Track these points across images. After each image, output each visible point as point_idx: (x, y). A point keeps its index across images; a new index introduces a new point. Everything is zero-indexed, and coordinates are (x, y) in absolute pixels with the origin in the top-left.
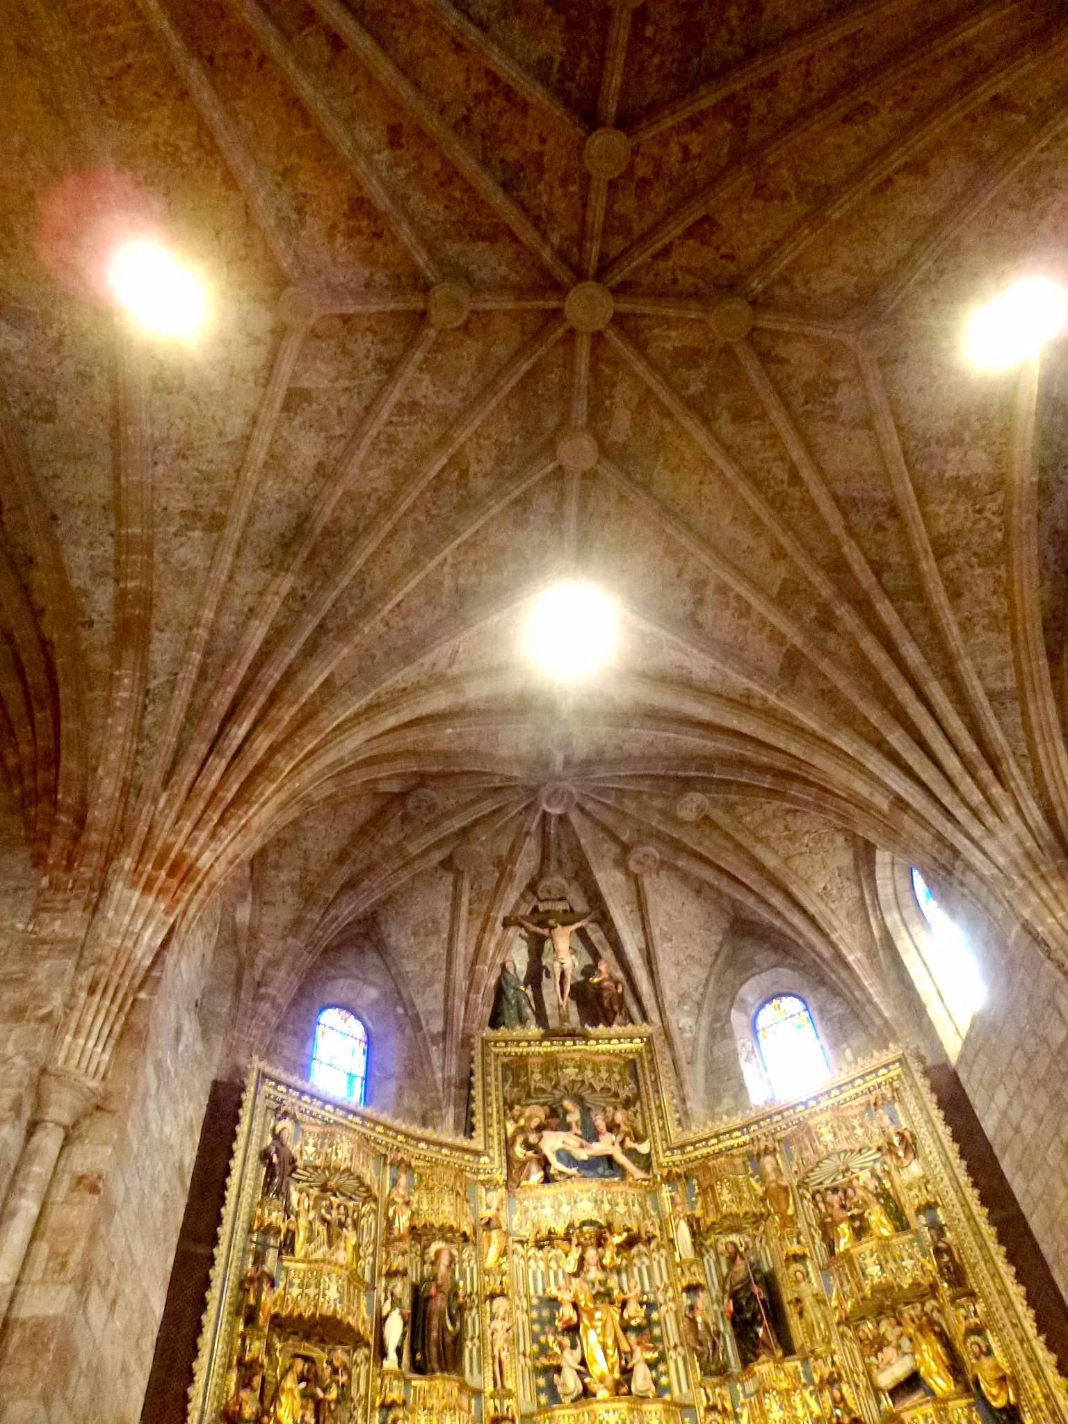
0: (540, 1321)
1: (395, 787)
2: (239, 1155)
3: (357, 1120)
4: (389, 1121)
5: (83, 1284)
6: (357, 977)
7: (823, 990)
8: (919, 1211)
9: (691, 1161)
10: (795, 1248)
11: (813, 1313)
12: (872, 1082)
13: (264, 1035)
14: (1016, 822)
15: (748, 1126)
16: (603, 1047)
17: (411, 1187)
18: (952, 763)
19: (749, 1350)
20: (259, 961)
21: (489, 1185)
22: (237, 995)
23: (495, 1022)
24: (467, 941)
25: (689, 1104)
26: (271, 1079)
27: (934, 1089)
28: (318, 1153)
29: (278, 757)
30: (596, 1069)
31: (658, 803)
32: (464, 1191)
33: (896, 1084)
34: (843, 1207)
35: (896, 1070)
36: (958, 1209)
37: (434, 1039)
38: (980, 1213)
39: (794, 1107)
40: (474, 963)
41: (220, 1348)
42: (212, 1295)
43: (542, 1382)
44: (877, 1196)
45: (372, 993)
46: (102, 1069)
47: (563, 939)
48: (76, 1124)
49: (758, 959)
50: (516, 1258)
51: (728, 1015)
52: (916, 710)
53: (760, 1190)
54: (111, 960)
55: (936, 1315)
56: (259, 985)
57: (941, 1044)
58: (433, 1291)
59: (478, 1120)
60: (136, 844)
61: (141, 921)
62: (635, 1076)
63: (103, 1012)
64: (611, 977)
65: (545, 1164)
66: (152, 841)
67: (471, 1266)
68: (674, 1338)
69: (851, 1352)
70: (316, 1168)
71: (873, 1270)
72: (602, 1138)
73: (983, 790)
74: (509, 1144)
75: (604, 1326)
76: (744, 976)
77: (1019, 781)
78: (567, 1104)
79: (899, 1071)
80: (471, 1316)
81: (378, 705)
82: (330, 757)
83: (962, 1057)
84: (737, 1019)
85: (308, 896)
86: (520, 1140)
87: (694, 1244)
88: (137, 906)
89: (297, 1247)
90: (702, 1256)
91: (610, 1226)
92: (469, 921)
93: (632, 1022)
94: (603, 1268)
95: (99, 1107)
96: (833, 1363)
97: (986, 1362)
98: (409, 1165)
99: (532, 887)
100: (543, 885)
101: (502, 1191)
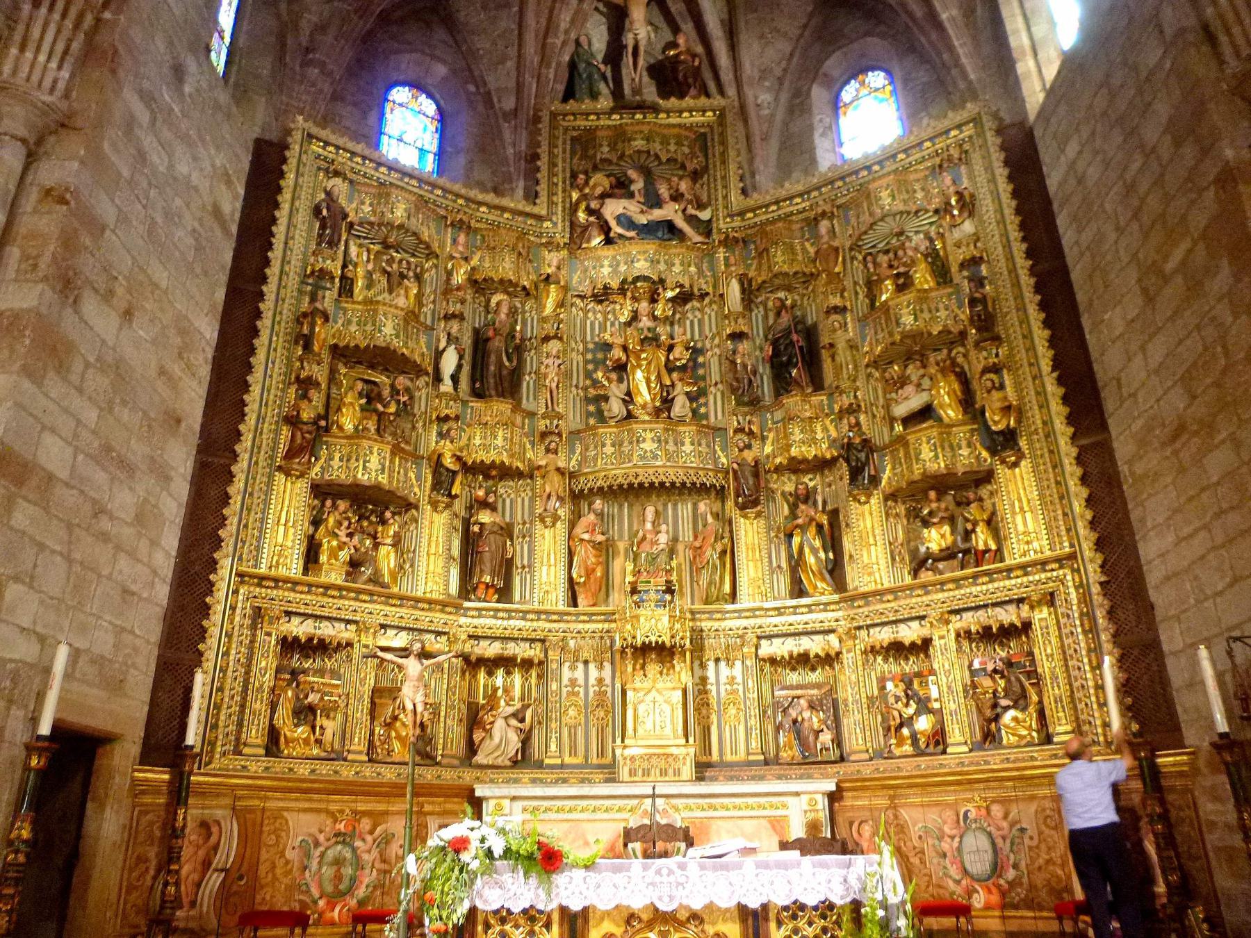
0: (595, 362)
3: (414, 182)
4: (448, 185)
6: (423, 52)
7: (911, 57)
8: (962, 266)
10: (836, 301)
11: (843, 354)
12: (940, 144)
15: (808, 193)
16: (674, 120)
17: (471, 248)
19: (782, 384)
21: (551, 245)
22: (281, 59)
23: (569, 95)
24: (537, 15)
25: (757, 177)
26: (319, 140)
27: (1003, 148)
28: (374, 212)
30: (665, 141)
32: (526, 253)
33: (966, 147)
34: (891, 267)
37: (507, 116)
38: (1023, 264)
39: (856, 172)
41: (277, 370)
42: (264, 324)
43: (592, 408)
44: (926, 256)
45: (441, 70)
46: (61, 85)
51: (810, 89)
53: (812, 250)
55: (960, 360)
56: (308, 50)
57: (1023, 101)
58: (491, 333)
59: (543, 188)
64: (688, 51)
65: (605, 229)
67: (532, 316)
68: (715, 376)
69: (875, 390)
70: (371, 224)
74: (574, 209)
75: (649, 364)
76: (831, 49)
78: (632, 174)
79: (972, 132)
80: (530, 357)
83: (1043, 112)
84: (818, 94)
86: (583, 206)
87: (743, 299)
89: (356, 291)
90: (751, 310)
91: (662, 281)
93: (708, 96)
94: (655, 318)
96: (856, 397)
97: (996, 395)
98: (469, 227)
101: (564, 253)
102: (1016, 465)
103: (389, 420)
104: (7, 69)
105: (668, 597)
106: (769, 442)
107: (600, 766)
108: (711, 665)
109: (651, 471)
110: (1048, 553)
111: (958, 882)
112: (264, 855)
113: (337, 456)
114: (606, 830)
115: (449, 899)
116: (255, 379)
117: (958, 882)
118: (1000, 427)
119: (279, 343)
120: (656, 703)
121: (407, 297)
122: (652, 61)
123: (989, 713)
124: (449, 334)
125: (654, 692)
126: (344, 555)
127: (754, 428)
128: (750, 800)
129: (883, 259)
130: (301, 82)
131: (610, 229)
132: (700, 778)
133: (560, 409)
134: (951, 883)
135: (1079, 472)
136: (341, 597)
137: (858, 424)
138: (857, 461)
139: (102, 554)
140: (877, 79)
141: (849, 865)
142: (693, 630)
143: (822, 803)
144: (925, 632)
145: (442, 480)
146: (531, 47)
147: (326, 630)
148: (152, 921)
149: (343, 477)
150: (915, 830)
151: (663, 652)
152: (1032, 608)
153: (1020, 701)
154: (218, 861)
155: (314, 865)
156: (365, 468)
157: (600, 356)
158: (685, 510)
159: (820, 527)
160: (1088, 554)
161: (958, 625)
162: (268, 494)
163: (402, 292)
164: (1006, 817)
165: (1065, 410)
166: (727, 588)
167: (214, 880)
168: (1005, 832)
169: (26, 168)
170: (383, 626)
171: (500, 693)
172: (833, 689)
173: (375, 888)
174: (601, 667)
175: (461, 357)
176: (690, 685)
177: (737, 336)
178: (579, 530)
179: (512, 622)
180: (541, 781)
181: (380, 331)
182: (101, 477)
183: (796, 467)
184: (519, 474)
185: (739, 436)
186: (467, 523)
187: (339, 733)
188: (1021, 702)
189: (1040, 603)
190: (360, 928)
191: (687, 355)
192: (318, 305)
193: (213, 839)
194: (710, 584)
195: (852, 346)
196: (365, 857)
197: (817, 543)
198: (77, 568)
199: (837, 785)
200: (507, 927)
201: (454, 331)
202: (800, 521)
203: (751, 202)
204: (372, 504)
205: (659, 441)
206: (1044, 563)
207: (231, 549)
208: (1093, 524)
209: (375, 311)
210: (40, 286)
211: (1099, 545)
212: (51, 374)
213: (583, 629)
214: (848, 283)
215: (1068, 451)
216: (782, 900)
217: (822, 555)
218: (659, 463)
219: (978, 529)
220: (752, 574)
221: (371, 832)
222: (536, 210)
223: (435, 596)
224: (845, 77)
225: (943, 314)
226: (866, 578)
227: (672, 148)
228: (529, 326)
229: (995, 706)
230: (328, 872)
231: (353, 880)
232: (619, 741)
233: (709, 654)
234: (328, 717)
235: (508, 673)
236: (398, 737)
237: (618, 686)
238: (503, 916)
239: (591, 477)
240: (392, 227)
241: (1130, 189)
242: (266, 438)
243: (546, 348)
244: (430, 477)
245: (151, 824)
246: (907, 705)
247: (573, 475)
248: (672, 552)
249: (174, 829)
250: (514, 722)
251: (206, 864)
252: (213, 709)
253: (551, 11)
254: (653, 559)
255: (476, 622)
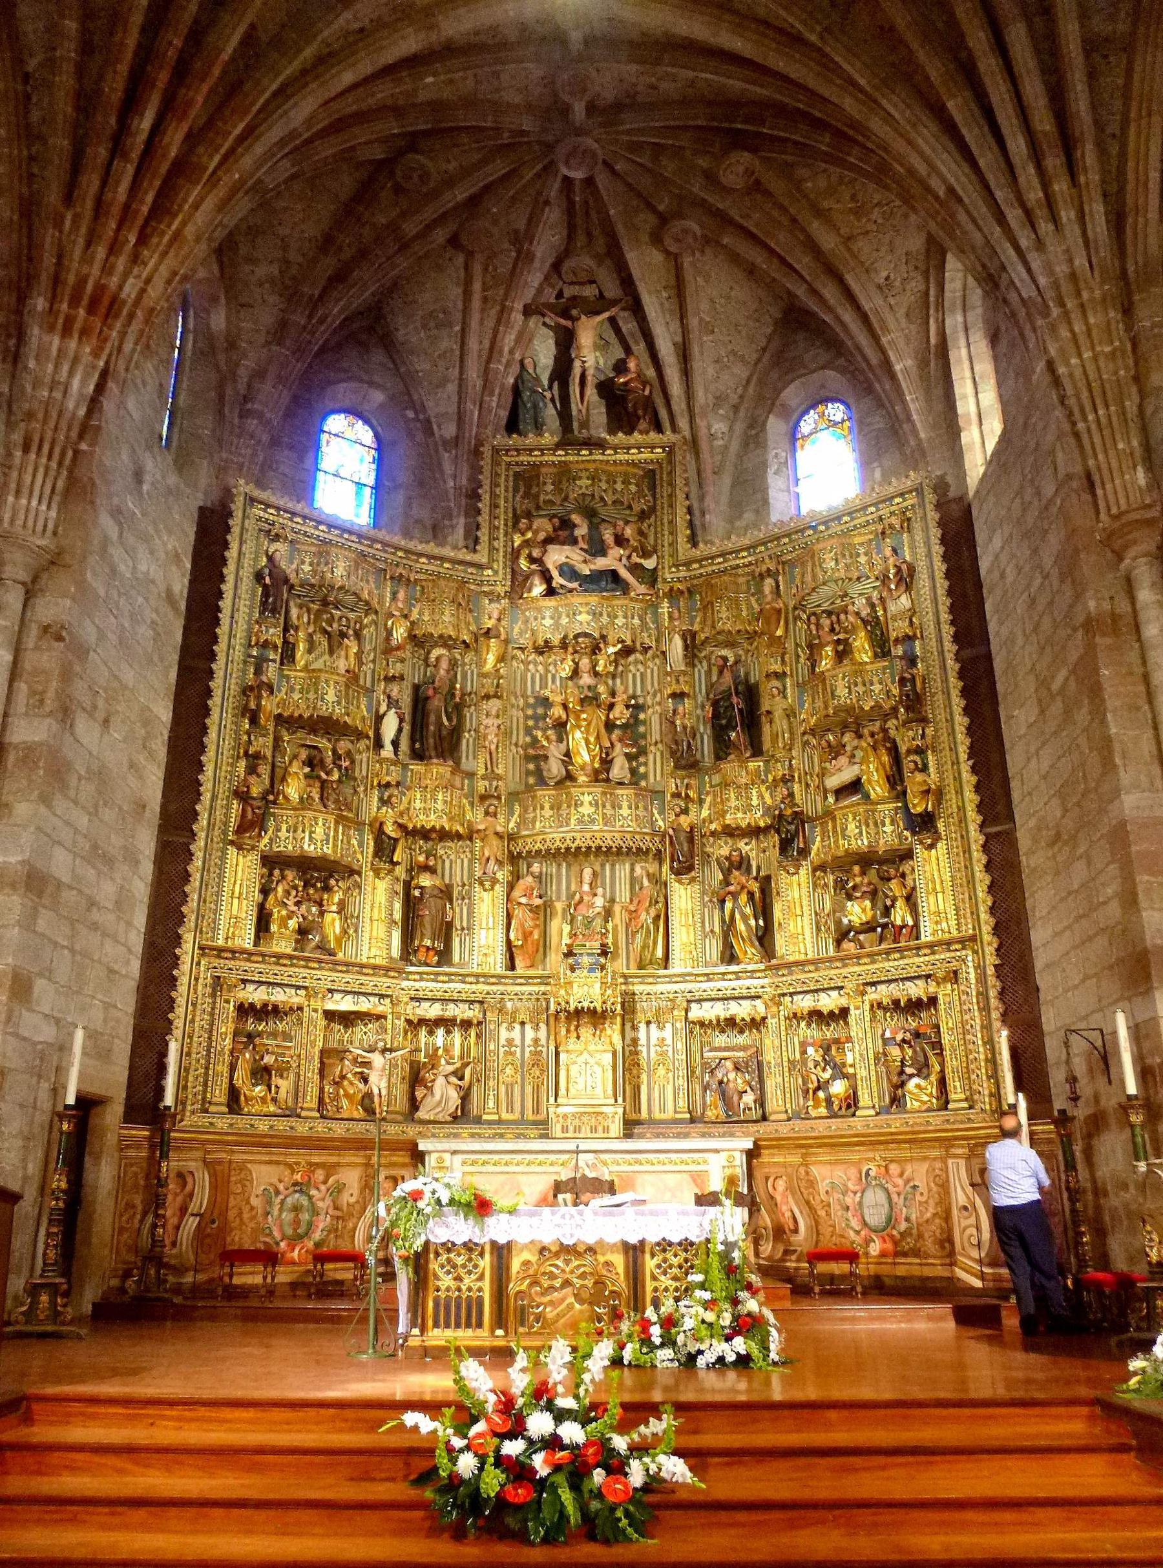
0: (535, 717)
1: (378, 153)
2: (230, 579)
3: (354, 538)
5: (65, 714)
9: (696, 577)
10: (777, 667)
11: (781, 723)
13: (254, 455)
14: (1073, 232)
15: (754, 547)
17: (410, 601)
18: (1018, 146)
20: (243, 373)
21: (494, 597)
22: (220, 412)
23: (512, 426)
26: (261, 503)
27: (941, 524)
28: (314, 571)
29: (201, 150)
30: (611, 481)
31: (703, 162)
34: (832, 630)
35: (912, 499)
36: (933, 643)
38: (950, 647)
40: (489, 360)
41: (227, 744)
42: (214, 703)
43: (531, 766)
44: (865, 622)
45: (378, 397)
46: (51, 526)
47: (588, 333)
48: (35, 579)
49: (807, 357)
50: (515, 663)
51: (764, 423)
52: (988, 65)
53: (757, 608)
54: (40, 416)
56: (246, 399)
58: (430, 692)
59: (483, 534)
60: (45, 278)
61: (66, 368)
62: (653, 488)
63: (41, 470)
65: (547, 578)
66: (63, 276)
68: (656, 736)
70: (313, 586)
71: (842, 691)
72: (611, 552)
73: (1046, 185)
74: (515, 554)
75: (589, 724)
77: (1091, 176)
78: (576, 518)
79: (915, 501)
81: (331, 55)
82: (274, 133)
83: (977, 492)
84: (775, 426)
85: (290, 293)
88: (59, 350)
89: (298, 655)
90: (694, 666)
92: (483, 310)
93: (659, 429)
94: (596, 674)
95: (54, 561)
97: (919, 777)
98: (409, 580)
99: (556, 267)
100: (566, 266)
102: (932, 846)
103: (332, 789)
104: (7, 517)
105: (602, 960)
106: (706, 806)
107: (535, 1123)
108: (643, 1026)
109: (588, 836)
110: (955, 933)
111: (858, 1232)
112: (232, 1203)
113: (284, 827)
114: (541, 1184)
115: (410, 1234)
116: (208, 759)
117: (858, 1232)
118: (919, 809)
119: (228, 718)
120: (588, 1065)
121: (347, 658)
122: (602, 378)
123: (895, 1079)
124: (389, 697)
125: (585, 1054)
126: (293, 924)
127: (691, 793)
128: (674, 1156)
129: (826, 622)
130: (239, 437)
131: (551, 578)
132: (628, 1135)
133: (500, 771)
134: (852, 1233)
135: (984, 859)
136: (292, 965)
137: (791, 795)
138: (789, 832)
139: (95, 939)
140: (836, 411)
141: (704, 1213)
142: (624, 994)
143: (740, 1160)
144: (843, 1002)
145: (384, 848)
146: (473, 373)
147: (279, 996)
148: (145, 1258)
149: (290, 847)
150: (823, 1186)
151: (596, 1017)
152: (938, 984)
153: (923, 1069)
154: (193, 1207)
155: (276, 1212)
156: (311, 838)
157: (540, 711)
158: (623, 870)
159: (751, 895)
160: (987, 938)
161: (874, 996)
162: (221, 868)
163: (343, 653)
164: (901, 1175)
165: (977, 799)
166: (660, 953)
167: (191, 1223)
168: (901, 1188)
169: (25, 606)
170: (330, 991)
171: (440, 1052)
172: (758, 1052)
173: (329, 1232)
174: (537, 1028)
175: (401, 721)
176: (619, 1048)
177: (678, 696)
178: (516, 893)
179: (452, 985)
180: (480, 1136)
181: (323, 699)
182: (91, 873)
183: (731, 832)
184: (459, 836)
185: (676, 801)
186: (407, 886)
187: (292, 1090)
188: (925, 1071)
189: (944, 979)
190: (319, 1267)
191: (628, 713)
192: (264, 679)
193: (189, 1187)
194: (643, 948)
195: (790, 714)
196: (320, 1204)
197: (748, 911)
198: (78, 958)
199: (755, 1143)
200: (452, 1255)
201: (394, 694)
202: (732, 888)
203: (696, 553)
204: (319, 874)
205: (597, 804)
206: (948, 943)
207: (193, 924)
208: (992, 910)
209: (317, 678)
210: (48, 720)
211: (997, 930)
212: (58, 796)
213: (520, 993)
214: (790, 645)
215: (976, 838)
216: (653, 1238)
217: (753, 922)
218: (596, 828)
219: (898, 904)
220: (685, 940)
221: (325, 1182)
222: (475, 558)
223: (378, 961)
224: (803, 407)
225: (877, 688)
226: (792, 948)
227: (619, 486)
228: (469, 681)
229: (902, 1072)
230: (287, 1216)
231: (310, 1224)
232: (552, 1100)
233: (640, 1017)
234: (281, 1077)
235: (448, 1032)
236: (347, 1095)
237: (552, 1048)
238: (449, 1247)
239: (529, 840)
240: (333, 588)
241: (1033, 602)
242: (219, 814)
243: (485, 706)
244: (372, 843)
245: (136, 1174)
246: (824, 1070)
247: (512, 837)
248: (608, 914)
249: (159, 1179)
250: (453, 1080)
251: (183, 1210)
252: (183, 1071)
253: (495, 337)
254: (589, 922)
255: (417, 985)
